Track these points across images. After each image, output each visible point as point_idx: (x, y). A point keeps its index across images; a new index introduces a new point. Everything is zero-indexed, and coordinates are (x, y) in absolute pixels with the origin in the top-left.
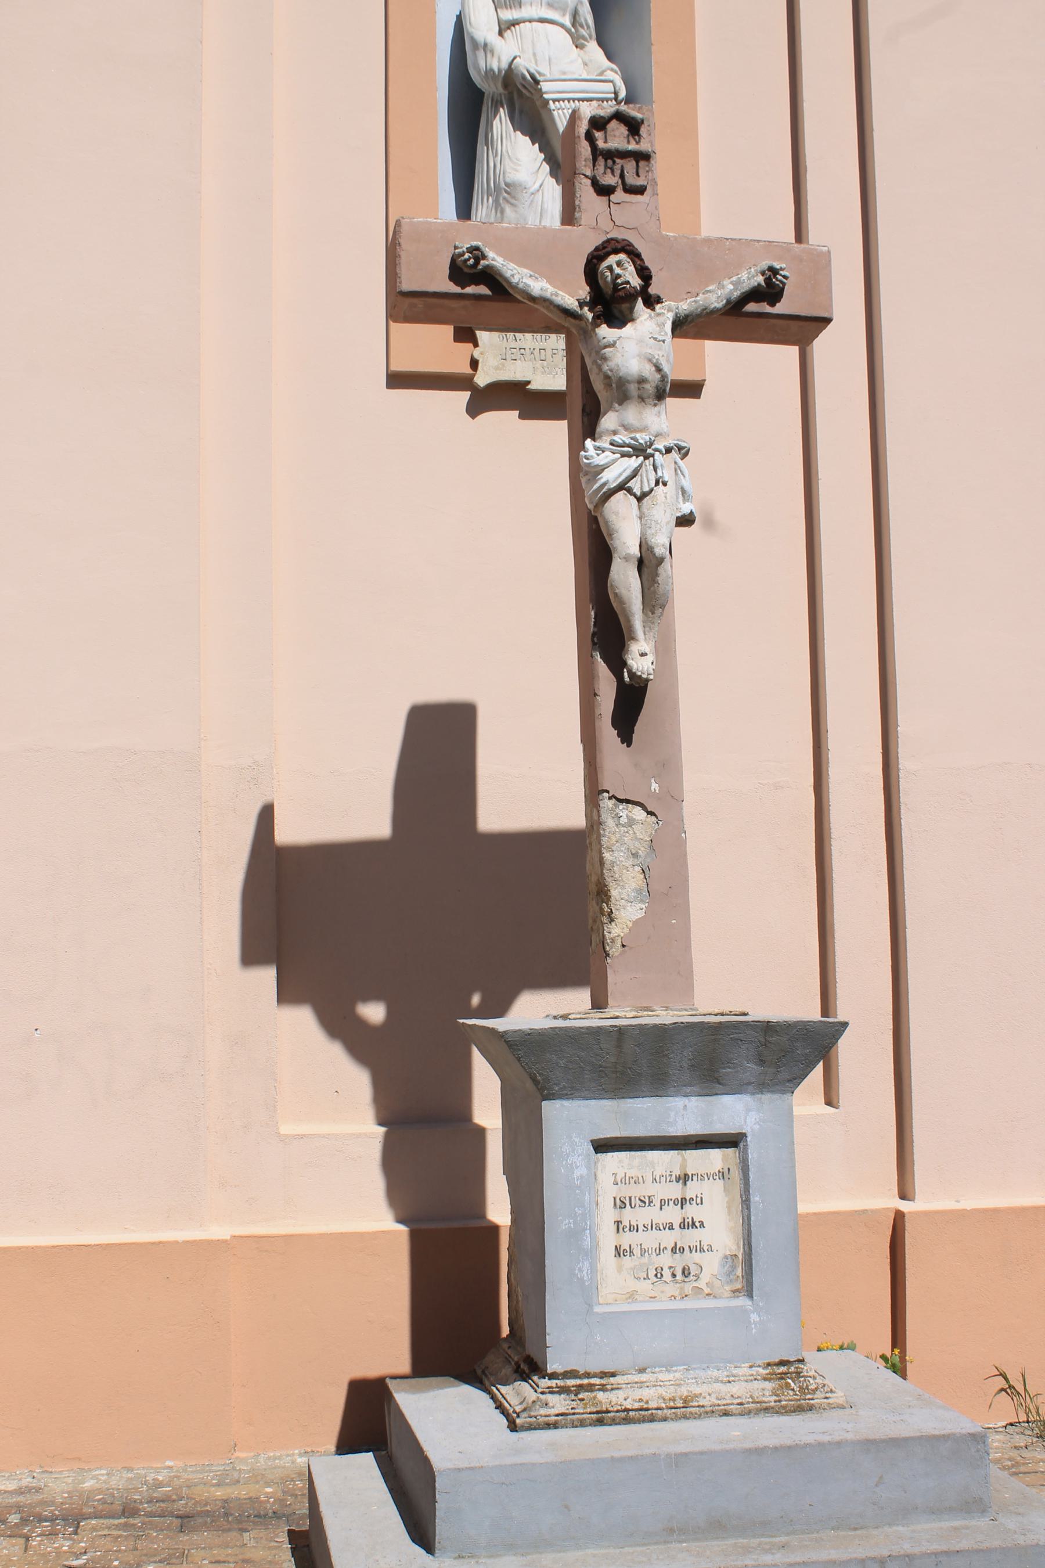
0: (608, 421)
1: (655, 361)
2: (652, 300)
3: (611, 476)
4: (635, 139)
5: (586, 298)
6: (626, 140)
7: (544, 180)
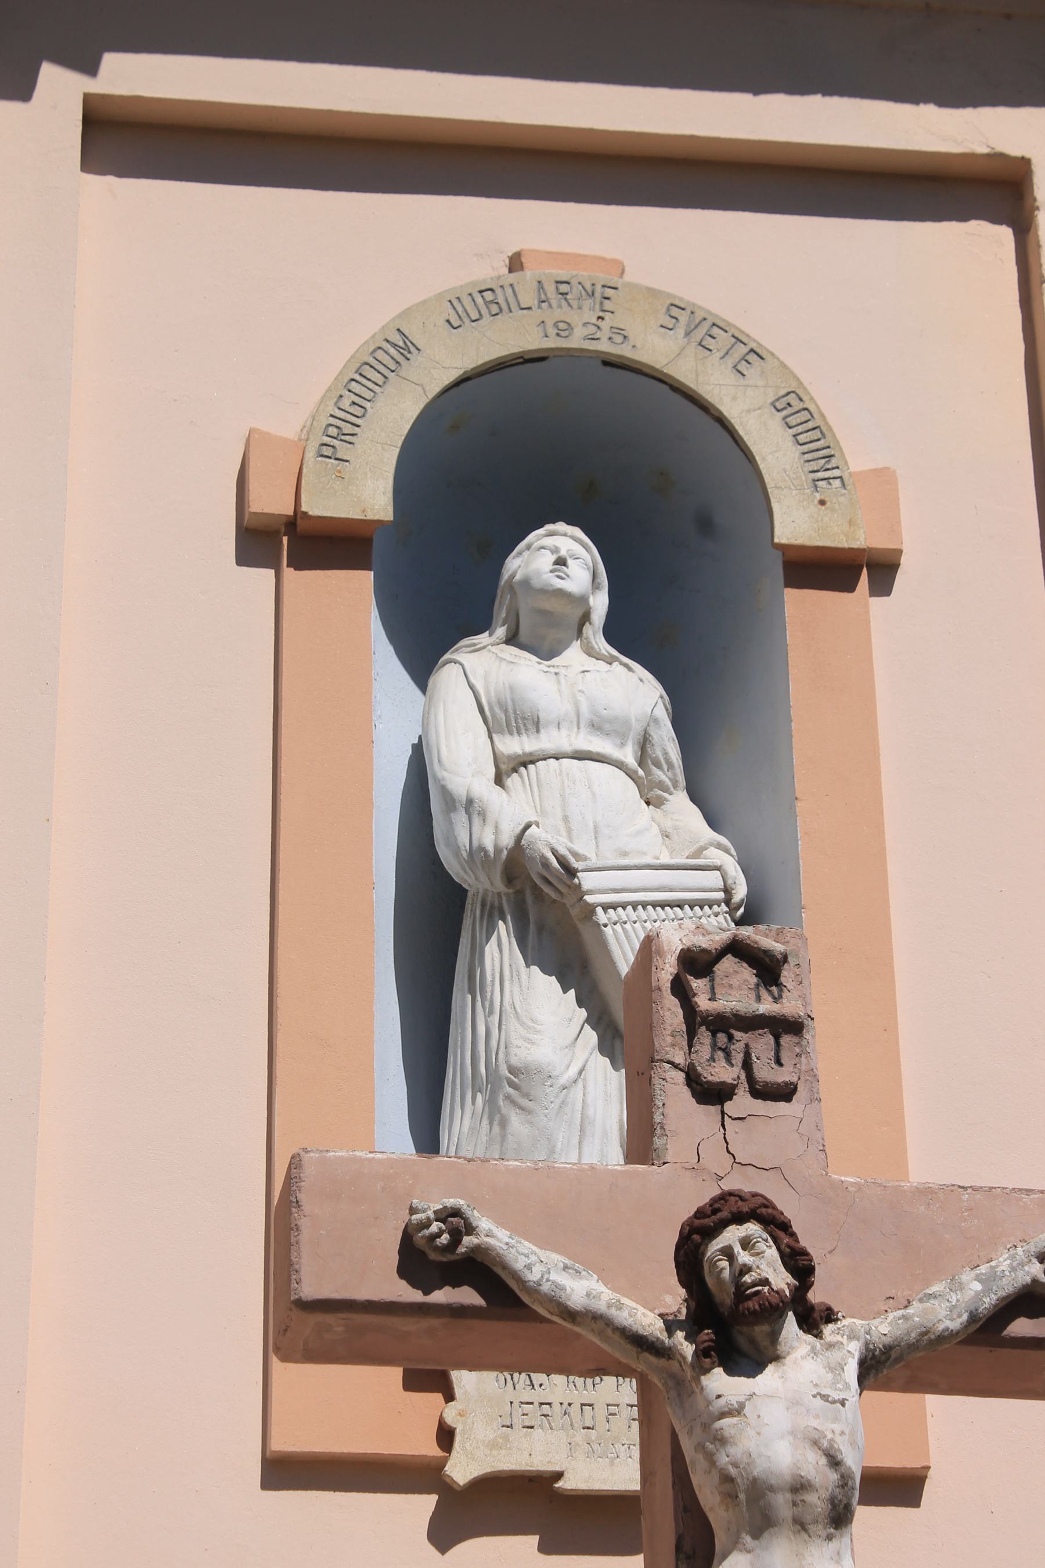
1: (826, 1444)
2: (816, 1315)
4: (770, 992)
5: (679, 1311)
6: (753, 995)
7: (587, 1061)
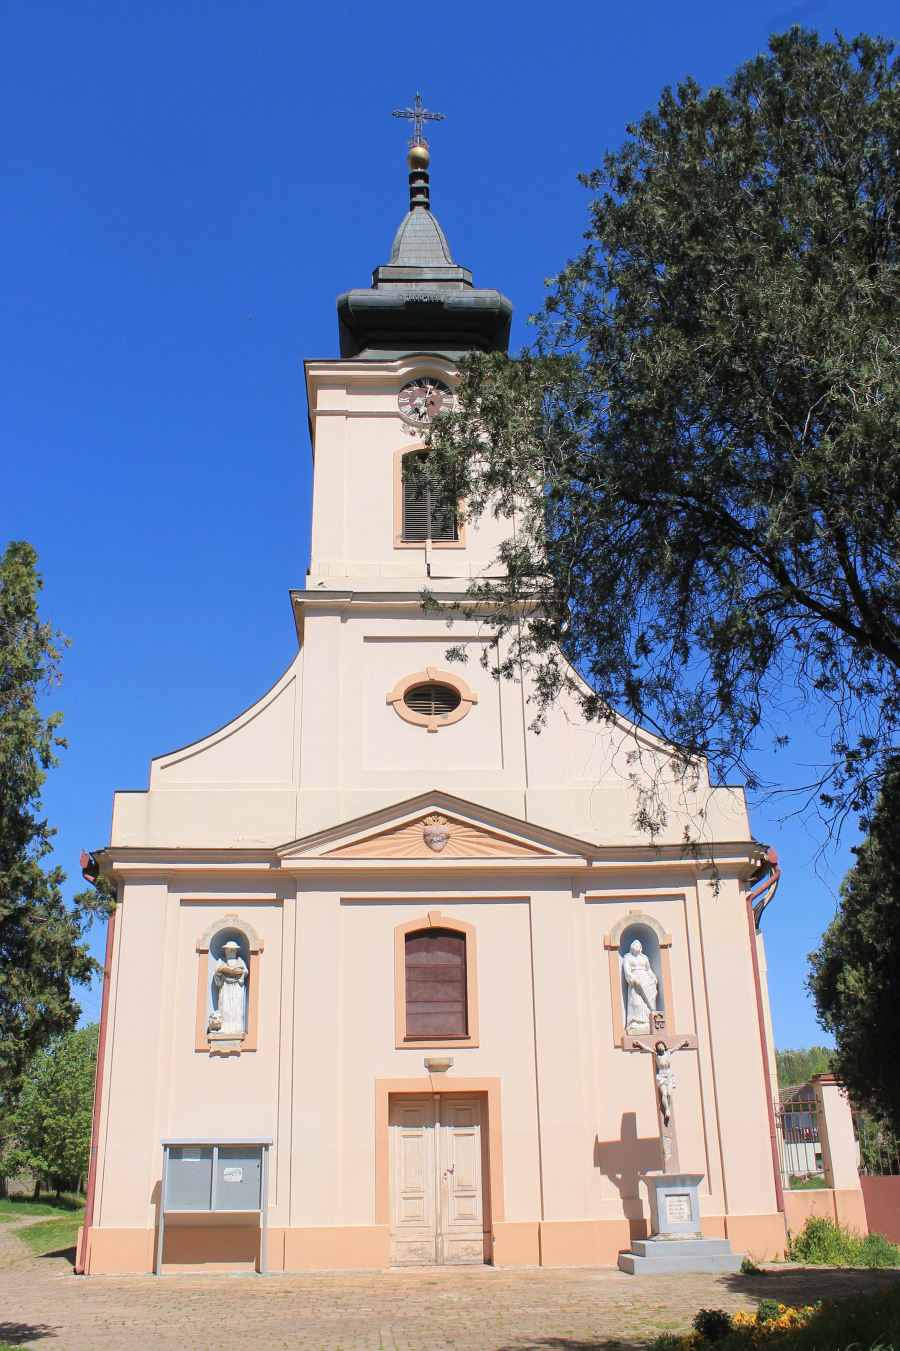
0: (660, 1072)
3: (661, 1082)
